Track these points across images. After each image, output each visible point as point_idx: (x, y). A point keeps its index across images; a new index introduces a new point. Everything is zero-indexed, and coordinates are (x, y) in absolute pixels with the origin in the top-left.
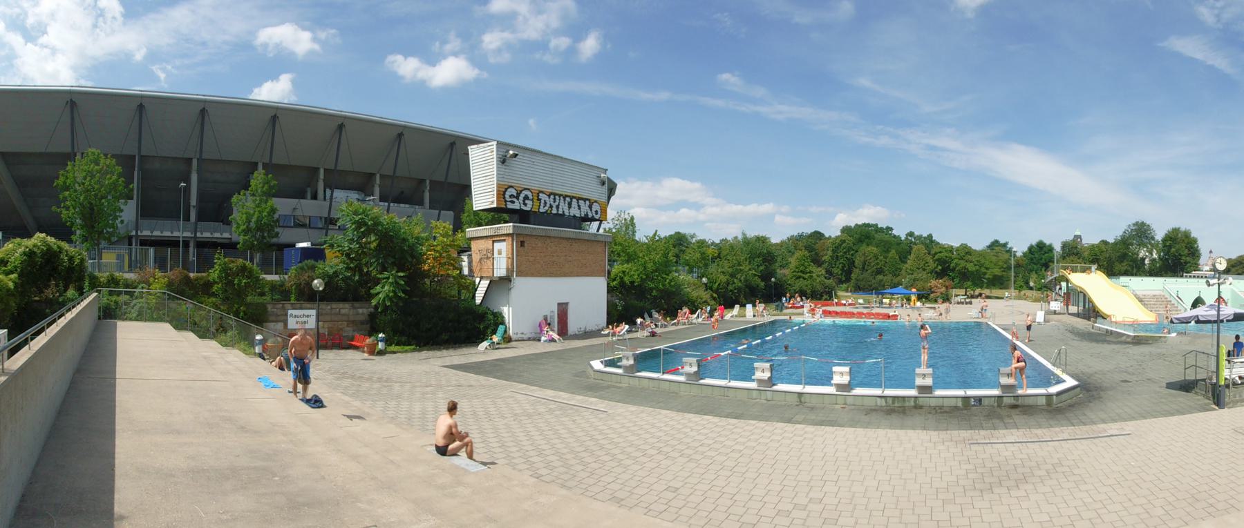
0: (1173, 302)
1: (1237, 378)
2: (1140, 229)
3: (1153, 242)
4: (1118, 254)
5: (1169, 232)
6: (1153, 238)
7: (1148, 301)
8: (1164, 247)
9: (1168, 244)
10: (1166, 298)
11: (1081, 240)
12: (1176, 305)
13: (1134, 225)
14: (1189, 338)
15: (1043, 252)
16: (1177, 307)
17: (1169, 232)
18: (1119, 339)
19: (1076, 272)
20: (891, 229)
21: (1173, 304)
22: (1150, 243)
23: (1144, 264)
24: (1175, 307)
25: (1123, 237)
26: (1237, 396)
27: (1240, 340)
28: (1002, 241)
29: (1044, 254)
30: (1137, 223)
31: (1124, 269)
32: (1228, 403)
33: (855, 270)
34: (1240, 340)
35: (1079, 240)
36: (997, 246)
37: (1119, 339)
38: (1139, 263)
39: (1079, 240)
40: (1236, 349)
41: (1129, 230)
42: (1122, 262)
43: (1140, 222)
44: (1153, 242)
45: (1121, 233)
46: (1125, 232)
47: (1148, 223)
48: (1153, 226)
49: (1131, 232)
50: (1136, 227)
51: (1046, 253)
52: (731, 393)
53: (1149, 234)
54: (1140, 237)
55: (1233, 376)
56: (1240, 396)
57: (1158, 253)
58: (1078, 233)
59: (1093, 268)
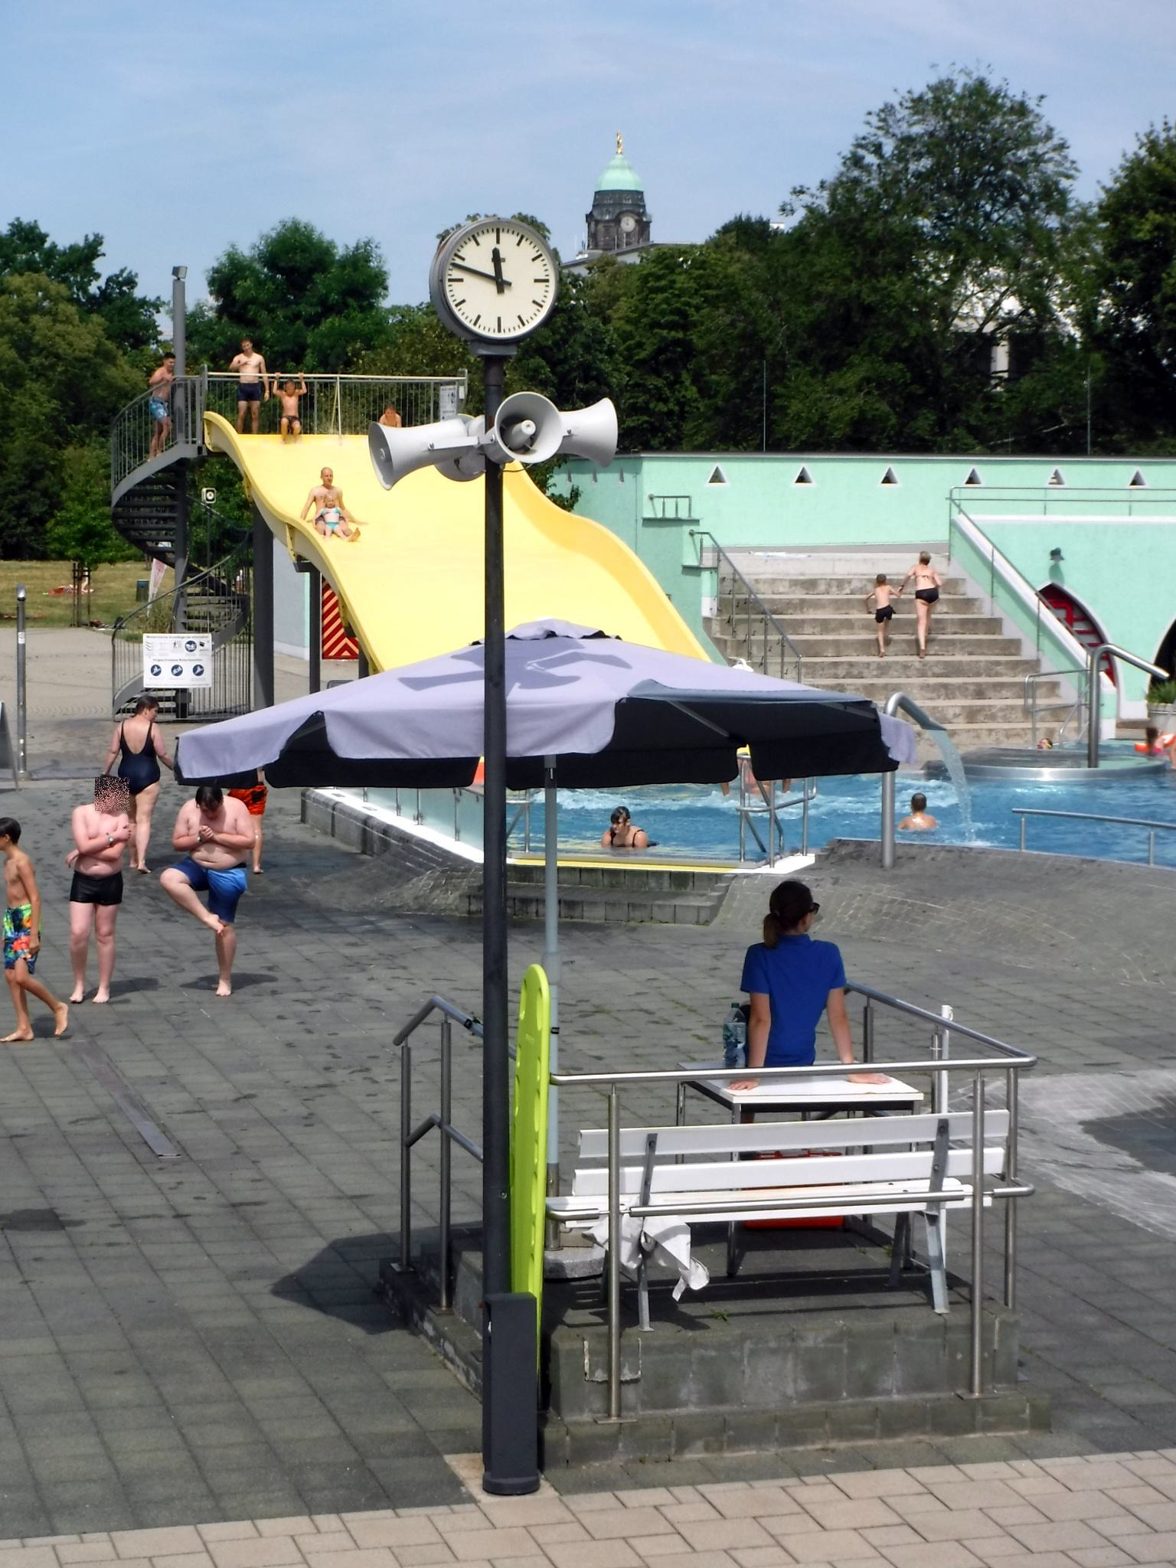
0: (1009, 632)
1: (680, 1247)
2: (952, 135)
3: (1053, 222)
4: (805, 315)
5: (1153, 146)
6: (1053, 196)
7: (825, 625)
8: (1115, 254)
9: (1143, 232)
10: (968, 603)
11: (643, 227)
12: (1028, 652)
13: (918, 105)
14: (885, 891)
15: (306, 310)
16: (1033, 666)
17: (1153, 146)
18: (387, 897)
19: (428, 423)
20: (131, 282)
21: (1013, 646)
22: (1031, 233)
23: (987, 374)
24: (1015, 666)
25: (844, 190)
26: (688, 1389)
27: (818, 930)
28: (63, 236)
29: (313, 321)
30: (941, 90)
31: (843, 409)
32: (586, 1450)
33: (142, 499)
34: (818, 930)
35: (629, 224)
36: (31, 266)
37: (387, 897)
38: (947, 371)
39: (629, 224)
40: (763, 1001)
41: (889, 147)
42: (834, 363)
43: (961, 83)
44: (1053, 222)
45: (831, 168)
46: (856, 161)
47: (1015, 92)
48: (1051, 115)
49: (901, 156)
50: (932, 123)
51: (328, 309)
52: (631, 1068)
53: (1021, 166)
54: (962, 190)
55: (654, 1227)
56: (717, 1393)
57: (1084, 294)
58: (619, 178)
59: (445, 393)
